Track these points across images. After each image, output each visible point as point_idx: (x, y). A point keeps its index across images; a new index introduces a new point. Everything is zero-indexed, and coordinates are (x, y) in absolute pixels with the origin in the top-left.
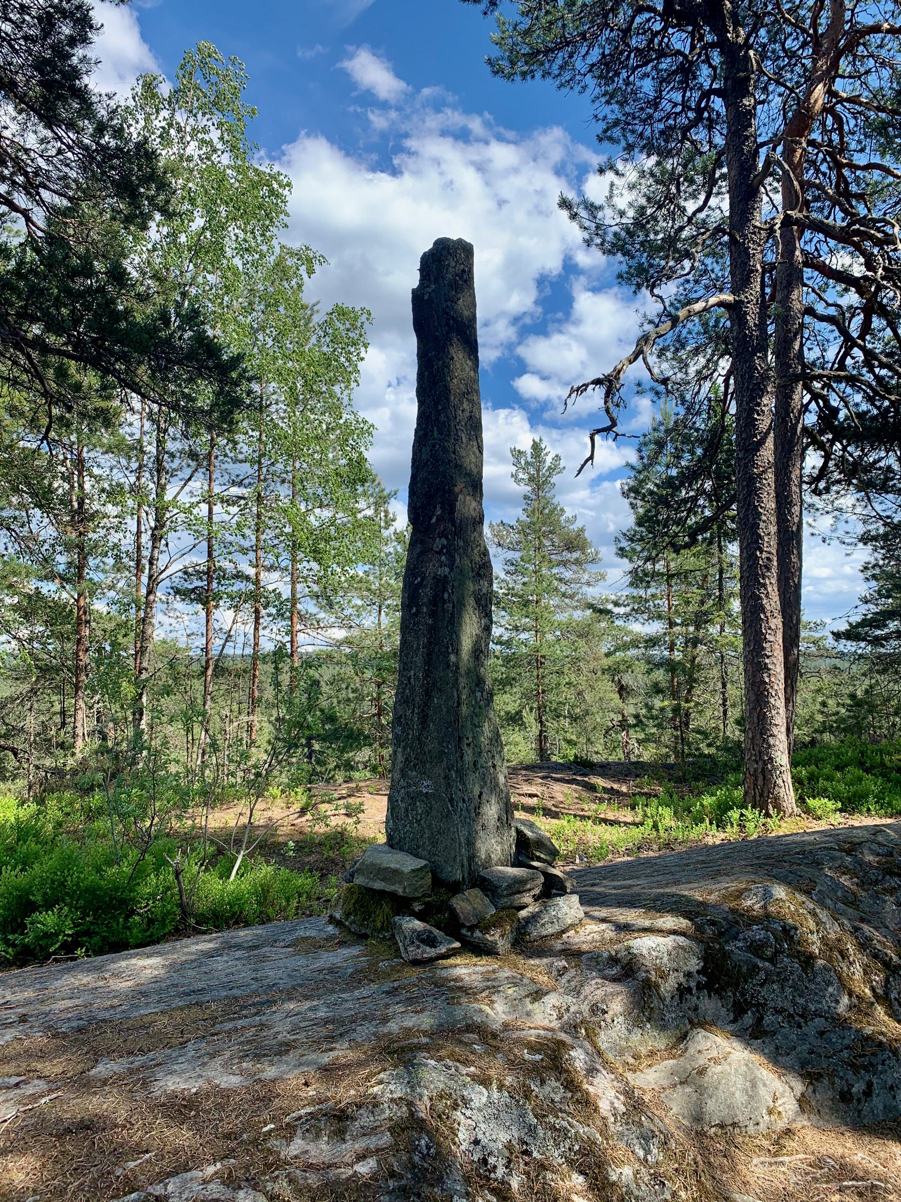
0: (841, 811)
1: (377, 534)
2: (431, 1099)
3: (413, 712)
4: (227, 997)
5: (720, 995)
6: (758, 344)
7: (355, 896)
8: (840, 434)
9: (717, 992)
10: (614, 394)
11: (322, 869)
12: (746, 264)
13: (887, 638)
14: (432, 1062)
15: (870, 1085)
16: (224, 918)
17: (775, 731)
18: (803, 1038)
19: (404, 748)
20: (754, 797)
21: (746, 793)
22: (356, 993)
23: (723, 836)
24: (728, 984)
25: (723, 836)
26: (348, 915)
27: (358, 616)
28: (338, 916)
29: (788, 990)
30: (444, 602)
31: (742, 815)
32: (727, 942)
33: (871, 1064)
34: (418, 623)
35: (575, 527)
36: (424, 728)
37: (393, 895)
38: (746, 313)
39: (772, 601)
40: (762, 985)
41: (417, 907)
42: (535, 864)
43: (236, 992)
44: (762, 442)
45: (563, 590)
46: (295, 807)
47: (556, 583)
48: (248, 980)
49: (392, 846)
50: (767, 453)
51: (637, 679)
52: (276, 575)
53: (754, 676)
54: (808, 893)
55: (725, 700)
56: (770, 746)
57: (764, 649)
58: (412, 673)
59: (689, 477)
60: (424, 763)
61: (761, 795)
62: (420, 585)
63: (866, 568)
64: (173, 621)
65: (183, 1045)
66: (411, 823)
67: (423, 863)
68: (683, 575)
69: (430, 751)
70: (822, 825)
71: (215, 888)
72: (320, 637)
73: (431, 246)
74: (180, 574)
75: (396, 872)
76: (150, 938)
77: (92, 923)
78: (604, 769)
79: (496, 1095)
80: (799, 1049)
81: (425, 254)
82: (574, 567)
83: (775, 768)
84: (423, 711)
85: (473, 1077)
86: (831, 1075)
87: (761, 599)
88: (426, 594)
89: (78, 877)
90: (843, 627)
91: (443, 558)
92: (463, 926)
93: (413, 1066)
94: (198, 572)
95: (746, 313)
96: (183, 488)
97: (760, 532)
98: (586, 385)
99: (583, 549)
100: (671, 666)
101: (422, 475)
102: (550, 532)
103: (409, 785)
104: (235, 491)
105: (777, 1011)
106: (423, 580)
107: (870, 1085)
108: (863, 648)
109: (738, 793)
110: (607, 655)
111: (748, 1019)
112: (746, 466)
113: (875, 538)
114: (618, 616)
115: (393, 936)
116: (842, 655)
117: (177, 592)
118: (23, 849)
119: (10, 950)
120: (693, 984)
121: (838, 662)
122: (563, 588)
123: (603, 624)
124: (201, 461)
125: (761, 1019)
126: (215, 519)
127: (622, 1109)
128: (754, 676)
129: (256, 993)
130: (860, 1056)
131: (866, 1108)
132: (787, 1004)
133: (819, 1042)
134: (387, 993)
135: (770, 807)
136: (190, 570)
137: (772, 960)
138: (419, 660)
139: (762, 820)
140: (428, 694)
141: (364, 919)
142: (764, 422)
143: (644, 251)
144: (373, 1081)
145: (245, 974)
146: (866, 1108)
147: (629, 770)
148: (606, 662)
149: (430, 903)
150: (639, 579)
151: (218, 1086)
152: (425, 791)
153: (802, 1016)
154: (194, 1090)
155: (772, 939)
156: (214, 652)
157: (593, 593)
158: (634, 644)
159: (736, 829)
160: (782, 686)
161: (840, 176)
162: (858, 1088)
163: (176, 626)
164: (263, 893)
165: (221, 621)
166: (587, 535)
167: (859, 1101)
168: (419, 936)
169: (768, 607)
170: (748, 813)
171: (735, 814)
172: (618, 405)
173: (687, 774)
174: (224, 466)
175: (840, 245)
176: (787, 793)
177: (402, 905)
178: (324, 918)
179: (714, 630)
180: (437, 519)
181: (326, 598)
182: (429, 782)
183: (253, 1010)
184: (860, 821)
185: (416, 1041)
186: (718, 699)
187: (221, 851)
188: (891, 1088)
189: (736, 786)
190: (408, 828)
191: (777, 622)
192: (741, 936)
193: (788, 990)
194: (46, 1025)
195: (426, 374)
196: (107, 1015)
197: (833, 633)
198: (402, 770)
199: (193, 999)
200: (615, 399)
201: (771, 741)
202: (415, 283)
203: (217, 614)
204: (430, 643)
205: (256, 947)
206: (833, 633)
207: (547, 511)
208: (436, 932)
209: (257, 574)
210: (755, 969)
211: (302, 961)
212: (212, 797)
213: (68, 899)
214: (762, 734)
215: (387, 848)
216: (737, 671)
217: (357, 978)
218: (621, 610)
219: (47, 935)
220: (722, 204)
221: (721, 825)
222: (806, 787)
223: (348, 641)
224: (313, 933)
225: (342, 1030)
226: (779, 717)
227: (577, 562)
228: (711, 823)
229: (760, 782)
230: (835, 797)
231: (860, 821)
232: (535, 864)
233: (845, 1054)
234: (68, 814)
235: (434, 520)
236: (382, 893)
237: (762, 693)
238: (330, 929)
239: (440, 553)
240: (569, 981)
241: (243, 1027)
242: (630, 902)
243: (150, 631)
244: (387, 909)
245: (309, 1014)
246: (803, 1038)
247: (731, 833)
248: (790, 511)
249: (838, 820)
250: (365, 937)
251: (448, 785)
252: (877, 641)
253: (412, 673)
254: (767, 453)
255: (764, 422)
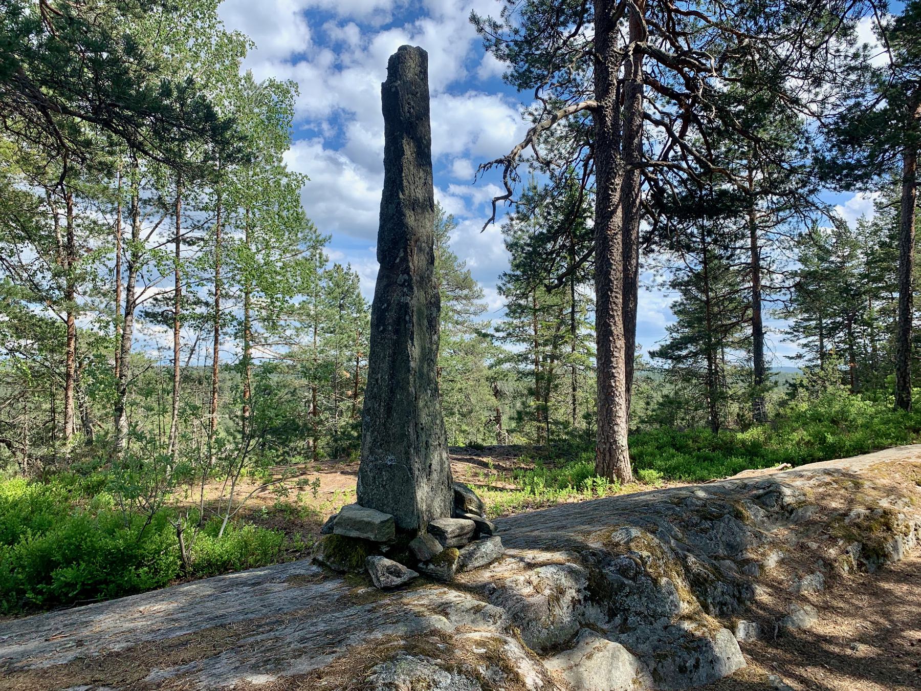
0: (663, 478)
1: (313, 271)
2: (412, 683)
3: (380, 405)
4: (243, 620)
5: (599, 604)
6: (609, 140)
7: (334, 543)
8: (663, 209)
9: (598, 603)
10: (511, 171)
11: (285, 529)
12: (606, 78)
13: (686, 357)
14: (410, 657)
15: (698, 661)
16: (213, 568)
17: (618, 421)
18: (654, 631)
19: (373, 432)
20: (603, 468)
21: (597, 466)
22: (345, 612)
23: (581, 497)
24: (605, 596)
25: (581, 497)
26: (328, 557)
27: (297, 336)
28: (320, 558)
29: (644, 599)
30: (406, 322)
31: (594, 482)
32: (603, 567)
33: (698, 647)
34: (384, 338)
35: (464, 270)
36: (388, 417)
37: (366, 541)
38: (605, 116)
39: (618, 328)
40: (627, 596)
41: (385, 549)
42: (468, 515)
43: (250, 616)
44: (614, 212)
45: (456, 318)
46: (258, 483)
47: (451, 313)
48: (258, 607)
49: (362, 505)
50: (618, 219)
51: (508, 387)
52: (230, 303)
53: (604, 382)
54: (653, 532)
55: (574, 400)
56: (614, 432)
57: (612, 362)
58: (379, 376)
59: (552, 236)
60: (388, 442)
61: (608, 467)
62: (386, 310)
63: (675, 306)
64: (147, 338)
65: (217, 655)
66: (378, 487)
67: (389, 516)
68: (546, 309)
69: (393, 434)
70: (649, 488)
71: (203, 546)
72: (266, 351)
73: (396, 51)
74: (151, 300)
75: (368, 523)
76: (157, 584)
77: (108, 574)
78: (490, 451)
79: (457, 678)
80: (651, 639)
81: (392, 57)
82: (464, 302)
83: (618, 448)
84: (388, 404)
85: (440, 666)
86: (673, 655)
87: (610, 326)
88: (391, 316)
89: (91, 541)
90: (657, 348)
91: (405, 289)
92: (420, 561)
93: (397, 660)
94: (166, 299)
95: (605, 116)
96: (154, 229)
97: (611, 277)
98: (491, 164)
99: (470, 288)
100: (538, 376)
101: (390, 225)
102: (447, 274)
103: (376, 460)
104: (197, 234)
105: (638, 614)
106: (388, 306)
107: (698, 661)
108: (668, 364)
109: (592, 466)
110: (490, 367)
111: (618, 620)
112: (602, 229)
113: (680, 284)
114: (498, 339)
115: (366, 571)
116: (652, 369)
117: (147, 314)
118: (36, 518)
119: (40, 597)
120: (581, 597)
121: (651, 374)
122: (456, 317)
123: (485, 345)
124: (171, 209)
125: (626, 619)
126: (182, 254)
127: (541, 683)
128: (604, 382)
129: (265, 616)
130: (692, 642)
131: (695, 676)
132: (643, 609)
133: (663, 634)
134: (369, 611)
135: (614, 475)
136: (159, 297)
137: (634, 579)
138: (385, 366)
139: (608, 485)
140: (392, 391)
141: (342, 560)
142: (616, 197)
143: (527, 62)
144: (369, 672)
145: (253, 604)
146: (695, 676)
147: (514, 451)
148: (491, 373)
149: (390, 548)
150: (514, 310)
151: (250, 683)
152: (389, 463)
153: (652, 617)
154: (232, 687)
155: (634, 564)
156: (181, 364)
157: (477, 321)
158: (509, 359)
159: (590, 492)
160: (624, 389)
161: (670, 18)
162: (690, 663)
163: (151, 343)
164: (244, 545)
165: (187, 338)
166: (472, 276)
167: (691, 671)
168: (388, 569)
169: (615, 332)
170: (598, 480)
171: (589, 481)
172: (514, 180)
173: (555, 453)
174: (188, 213)
175: (667, 69)
176: (626, 467)
177: (373, 548)
178: (309, 559)
179: (567, 349)
180: (401, 260)
181: (271, 323)
182: (393, 457)
183: (268, 628)
184: (672, 485)
185: (396, 643)
186: (569, 399)
187: (208, 517)
188: (711, 662)
189: (588, 460)
190: (375, 491)
191: (621, 343)
192: (613, 563)
193: (644, 599)
194: (100, 647)
195: (392, 148)
196: (150, 638)
197: (650, 352)
198: (370, 449)
199: (218, 622)
200: (513, 175)
201: (616, 428)
202: (385, 80)
203: (183, 332)
204: (394, 353)
205: (259, 584)
206: (650, 352)
207: (443, 258)
208: (400, 566)
209: (217, 302)
210: (622, 586)
211: (297, 592)
212: (186, 476)
213: (86, 558)
214: (609, 423)
215: (358, 507)
216: (592, 378)
217: (344, 602)
218: (501, 334)
219: (67, 584)
220: (589, 32)
221: (580, 489)
222: (639, 463)
223: (290, 356)
224: (303, 572)
225: (339, 638)
226: (621, 412)
227: (466, 297)
228: (573, 488)
229: (607, 458)
230: (660, 470)
231: (672, 485)
232: (468, 515)
233: (682, 640)
234: (70, 491)
235: (398, 260)
236: (357, 540)
237: (610, 394)
238: (314, 568)
239: (403, 285)
240: (497, 598)
241: (262, 640)
242: (533, 544)
243: (128, 345)
244: (361, 551)
245: (312, 628)
246: (654, 631)
247: (588, 495)
248: (630, 263)
249: (660, 484)
250: (343, 573)
251: (408, 459)
252: (679, 359)
253: (379, 376)
254: (618, 219)
255: (616, 197)
